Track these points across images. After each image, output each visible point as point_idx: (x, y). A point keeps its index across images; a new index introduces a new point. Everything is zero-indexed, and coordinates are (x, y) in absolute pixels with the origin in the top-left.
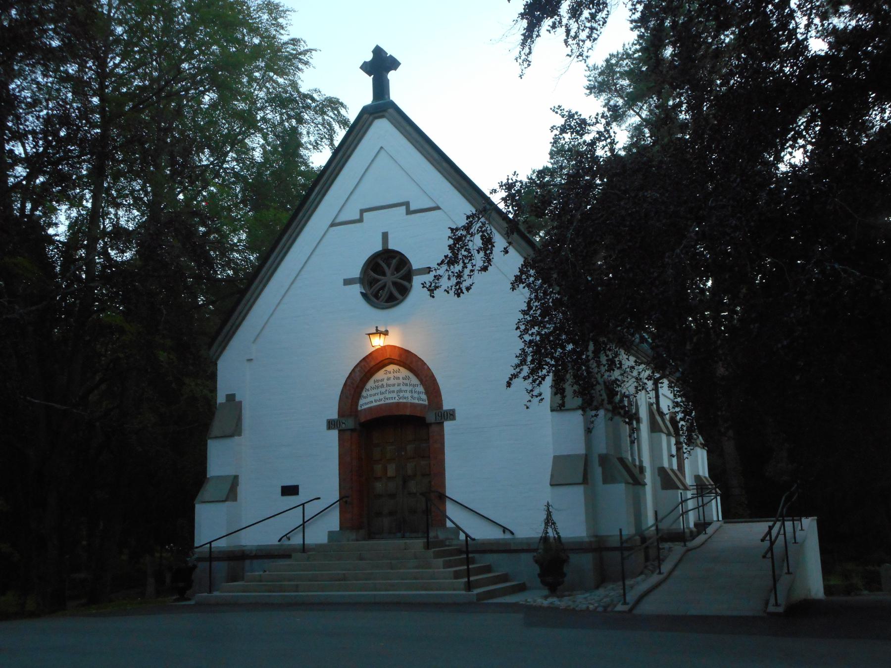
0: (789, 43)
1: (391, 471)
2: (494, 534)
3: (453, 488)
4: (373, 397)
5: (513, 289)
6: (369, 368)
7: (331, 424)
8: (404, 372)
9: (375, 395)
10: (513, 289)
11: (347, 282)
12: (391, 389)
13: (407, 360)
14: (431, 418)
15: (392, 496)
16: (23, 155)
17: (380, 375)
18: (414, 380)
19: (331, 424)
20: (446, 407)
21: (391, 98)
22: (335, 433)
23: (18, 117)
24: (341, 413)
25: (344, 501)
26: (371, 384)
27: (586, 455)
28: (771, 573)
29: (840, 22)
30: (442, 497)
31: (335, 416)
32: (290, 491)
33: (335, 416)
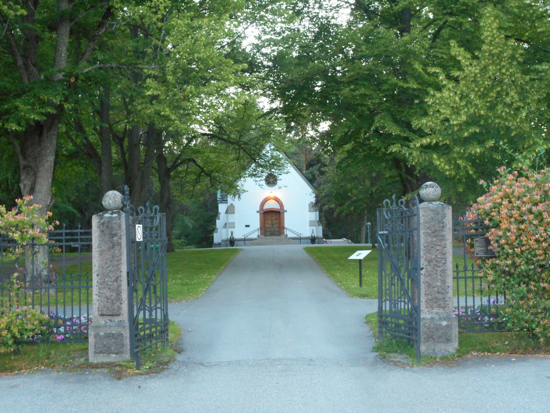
1: (270, 222)
4: (267, 206)
6: (266, 200)
7: (258, 212)
8: (275, 201)
11: (281, 180)
12: (272, 205)
13: (277, 200)
14: (281, 211)
15: (270, 228)
16: (45, 118)
17: (268, 201)
18: (277, 203)
19: (258, 212)
22: (259, 214)
23: (176, 136)
24: (260, 210)
25: (261, 228)
26: (266, 203)
27: (100, 326)
28: (363, 278)
29: (476, 69)
30: (284, 228)
32: (247, 226)
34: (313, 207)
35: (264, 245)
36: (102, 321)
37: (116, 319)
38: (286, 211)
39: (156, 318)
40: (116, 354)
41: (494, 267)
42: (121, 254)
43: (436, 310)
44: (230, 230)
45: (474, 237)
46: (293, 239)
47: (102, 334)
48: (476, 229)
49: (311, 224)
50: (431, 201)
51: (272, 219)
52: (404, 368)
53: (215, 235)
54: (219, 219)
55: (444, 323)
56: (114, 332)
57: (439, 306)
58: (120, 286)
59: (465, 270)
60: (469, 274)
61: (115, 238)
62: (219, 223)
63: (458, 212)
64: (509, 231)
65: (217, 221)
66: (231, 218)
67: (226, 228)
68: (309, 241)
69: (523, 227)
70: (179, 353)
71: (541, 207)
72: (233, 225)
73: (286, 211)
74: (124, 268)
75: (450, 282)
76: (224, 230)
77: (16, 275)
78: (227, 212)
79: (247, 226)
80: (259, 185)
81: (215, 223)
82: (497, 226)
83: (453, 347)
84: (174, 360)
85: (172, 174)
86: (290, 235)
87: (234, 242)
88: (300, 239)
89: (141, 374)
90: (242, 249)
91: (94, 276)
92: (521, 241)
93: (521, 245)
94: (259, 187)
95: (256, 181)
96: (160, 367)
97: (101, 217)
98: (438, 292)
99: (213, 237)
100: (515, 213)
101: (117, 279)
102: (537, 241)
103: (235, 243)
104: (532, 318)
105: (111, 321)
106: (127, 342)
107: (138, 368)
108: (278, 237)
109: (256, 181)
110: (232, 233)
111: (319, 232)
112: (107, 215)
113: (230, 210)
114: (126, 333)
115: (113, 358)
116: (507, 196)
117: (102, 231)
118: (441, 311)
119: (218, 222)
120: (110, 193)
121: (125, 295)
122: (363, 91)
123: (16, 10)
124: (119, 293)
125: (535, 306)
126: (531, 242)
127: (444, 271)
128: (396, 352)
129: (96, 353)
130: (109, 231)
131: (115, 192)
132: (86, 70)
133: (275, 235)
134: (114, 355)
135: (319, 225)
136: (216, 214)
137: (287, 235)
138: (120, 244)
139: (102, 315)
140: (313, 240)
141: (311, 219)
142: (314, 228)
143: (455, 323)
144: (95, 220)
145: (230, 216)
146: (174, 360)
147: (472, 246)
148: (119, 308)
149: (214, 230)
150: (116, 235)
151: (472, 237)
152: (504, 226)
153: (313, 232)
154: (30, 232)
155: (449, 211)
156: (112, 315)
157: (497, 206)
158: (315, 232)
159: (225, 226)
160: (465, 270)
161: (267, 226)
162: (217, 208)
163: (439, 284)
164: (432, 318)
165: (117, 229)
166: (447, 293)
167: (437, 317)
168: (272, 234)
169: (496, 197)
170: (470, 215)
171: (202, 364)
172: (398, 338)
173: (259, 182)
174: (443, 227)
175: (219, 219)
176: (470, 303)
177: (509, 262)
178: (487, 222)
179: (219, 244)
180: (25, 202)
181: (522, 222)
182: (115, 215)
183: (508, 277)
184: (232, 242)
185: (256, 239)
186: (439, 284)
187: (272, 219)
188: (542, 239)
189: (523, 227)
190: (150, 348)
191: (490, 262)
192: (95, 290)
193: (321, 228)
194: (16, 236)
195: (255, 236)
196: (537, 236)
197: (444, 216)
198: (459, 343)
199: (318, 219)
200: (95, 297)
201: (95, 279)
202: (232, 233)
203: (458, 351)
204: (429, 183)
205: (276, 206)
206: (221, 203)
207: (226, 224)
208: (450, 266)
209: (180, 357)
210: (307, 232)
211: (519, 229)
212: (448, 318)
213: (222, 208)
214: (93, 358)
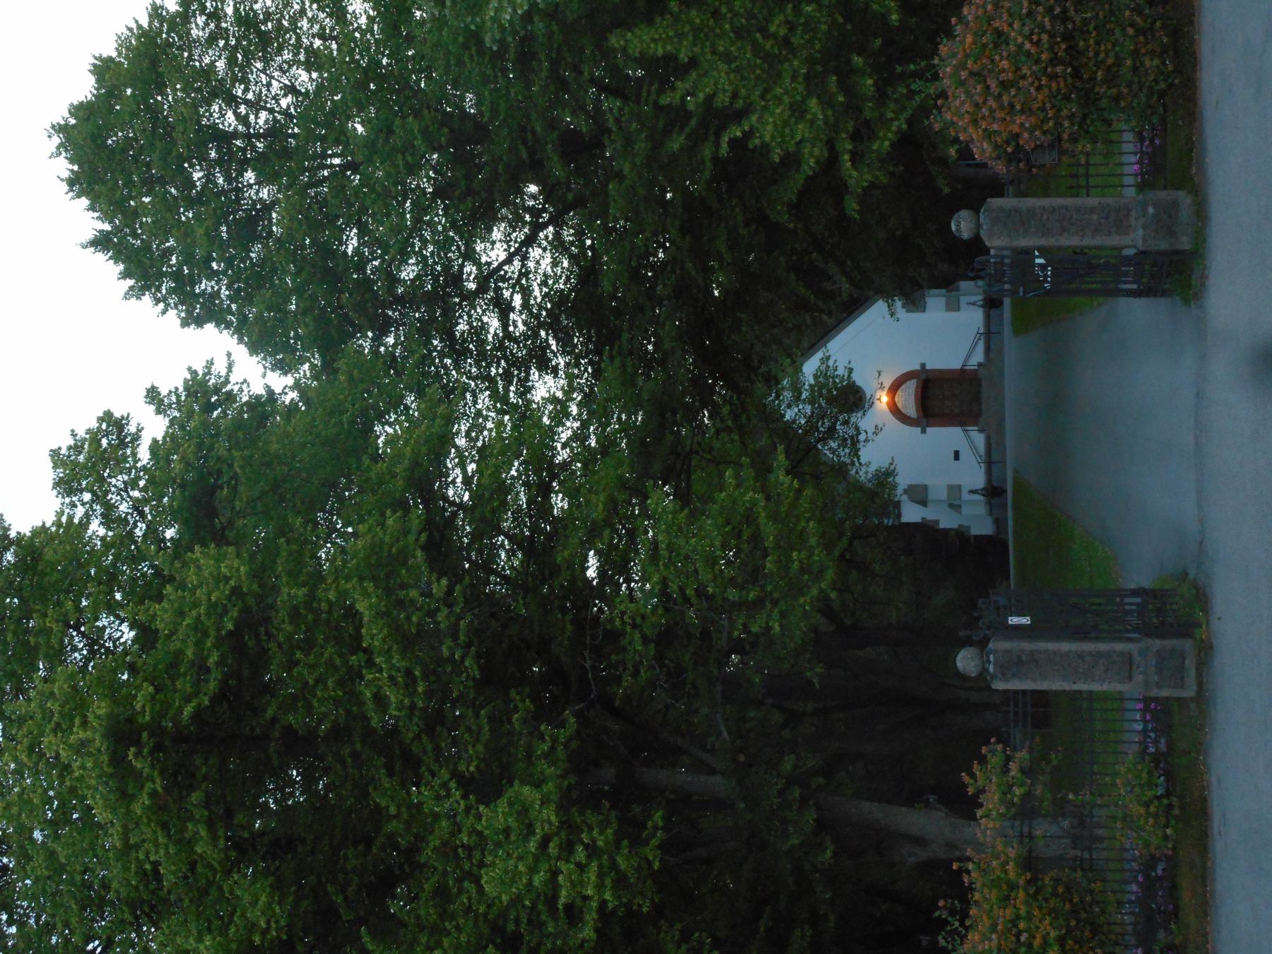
0: (716, 159)
1: (948, 403)
2: (981, 345)
3: (956, 365)
4: (911, 411)
5: (189, 369)
7: (924, 431)
8: (899, 392)
9: (649, 92)
10: (189, 369)
12: (907, 399)
13: (894, 389)
14: (923, 376)
17: (899, 405)
19: (924, 431)
20: (918, 368)
21: (879, 308)
22: (928, 429)
24: (917, 426)
25: (963, 424)
30: (962, 371)
31: (919, 429)
32: (957, 455)
33: (919, 429)
34: (914, 304)
35: (1002, 419)
36: (1139, 678)
37: (1137, 658)
38: (923, 365)
39: (1137, 604)
40: (1184, 659)
41: (1074, 140)
42: (1047, 651)
43: (1132, 221)
44: (966, 496)
45: (1028, 171)
46: (988, 349)
47: (1156, 678)
48: (1019, 161)
49: (953, 306)
50: (978, 226)
51: (940, 398)
52: (1207, 277)
53: (976, 531)
54: (937, 522)
55: (1151, 210)
56: (1154, 662)
57: (1127, 216)
58: (1090, 654)
59: (1075, 176)
60: (1082, 171)
61: (1024, 658)
62: (948, 521)
63: (997, 188)
64: (1022, 124)
65: (942, 525)
66: (938, 491)
67: (960, 506)
68: (993, 312)
69: (1018, 107)
70: (1186, 574)
71: (993, 83)
72: (955, 490)
73: (923, 365)
74: (1066, 646)
75: (1092, 201)
76: (965, 510)
77: (1071, 796)
78: (924, 503)
79: (957, 455)
80: (876, 433)
81: (946, 532)
82: (1017, 136)
83: (1184, 198)
84: (1195, 580)
85: (848, 621)
86: (978, 357)
87: (993, 487)
88: (990, 335)
89: (1208, 621)
90: (1016, 471)
91: (1075, 687)
92: (1038, 109)
93: (1043, 109)
94: (881, 435)
95: (866, 441)
96: (1201, 598)
97: (994, 677)
98: (1107, 218)
99: (976, 537)
100: (999, 115)
101: (1081, 656)
102: (1039, 89)
103: (995, 484)
104: (1145, 90)
105: (1138, 667)
106: (1169, 643)
107: (1200, 625)
108: (984, 383)
109: (866, 441)
110: (973, 492)
111: (971, 292)
112: (991, 668)
113: (919, 495)
114: (1157, 644)
115: (1190, 663)
116: (975, 122)
117: (1014, 675)
118: (1133, 214)
119: (943, 525)
120: (960, 664)
121: (1103, 647)
122: (721, 246)
123: (656, 828)
124: (1100, 655)
125: (1129, 85)
126: (1040, 97)
127: (1078, 210)
128: (1190, 276)
129: (1182, 687)
130: (1015, 665)
131: (959, 658)
132: (725, 734)
133: (980, 392)
134: (1187, 663)
135: (958, 289)
136: (926, 529)
137: (980, 365)
138: (1032, 652)
139: (1130, 678)
140: (991, 304)
141: (943, 306)
142: (964, 300)
143: (1151, 195)
144: (999, 685)
145: (932, 495)
146: (1195, 580)
147: (1042, 166)
148: (1121, 654)
149: (961, 535)
150: (1019, 657)
151: (1030, 166)
152: (1016, 129)
153: (974, 304)
154: (1012, 773)
155: (995, 202)
156: (1131, 664)
157: (988, 134)
158: (973, 299)
159: (955, 507)
160: (1075, 176)
161: (957, 411)
162: (908, 524)
163: (1095, 217)
164: (1144, 227)
165: (1007, 657)
166: (1111, 209)
167: (1142, 221)
168: (977, 398)
169: (975, 134)
170: (1000, 168)
171: (1201, 543)
172: (1173, 273)
173: (870, 434)
174: (1016, 211)
175: (937, 522)
176: (1127, 169)
177: (1066, 124)
178: (1009, 150)
179: (999, 522)
180: (972, 781)
181: (1012, 106)
182: (992, 658)
183: (1088, 122)
184: (993, 492)
185: (988, 439)
186: (1095, 217)
187: (940, 398)
188: (1036, 84)
189: (1018, 107)
190: (1175, 614)
191: (1066, 145)
192: (1095, 687)
193: (964, 285)
194: (1018, 791)
195: (979, 439)
196: (1032, 90)
197: (1001, 209)
198: (1178, 189)
199: (944, 291)
200: (1106, 687)
201: (1082, 686)
202: (973, 492)
203: (1189, 192)
204: (954, 228)
205: (911, 388)
206: (899, 516)
207: (951, 506)
208: (1069, 201)
209: (1192, 573)
210: (972, 318)
211: (1022, 111)
212: (1144, 206)
213: (911, 514)
214: (1190, 692)
